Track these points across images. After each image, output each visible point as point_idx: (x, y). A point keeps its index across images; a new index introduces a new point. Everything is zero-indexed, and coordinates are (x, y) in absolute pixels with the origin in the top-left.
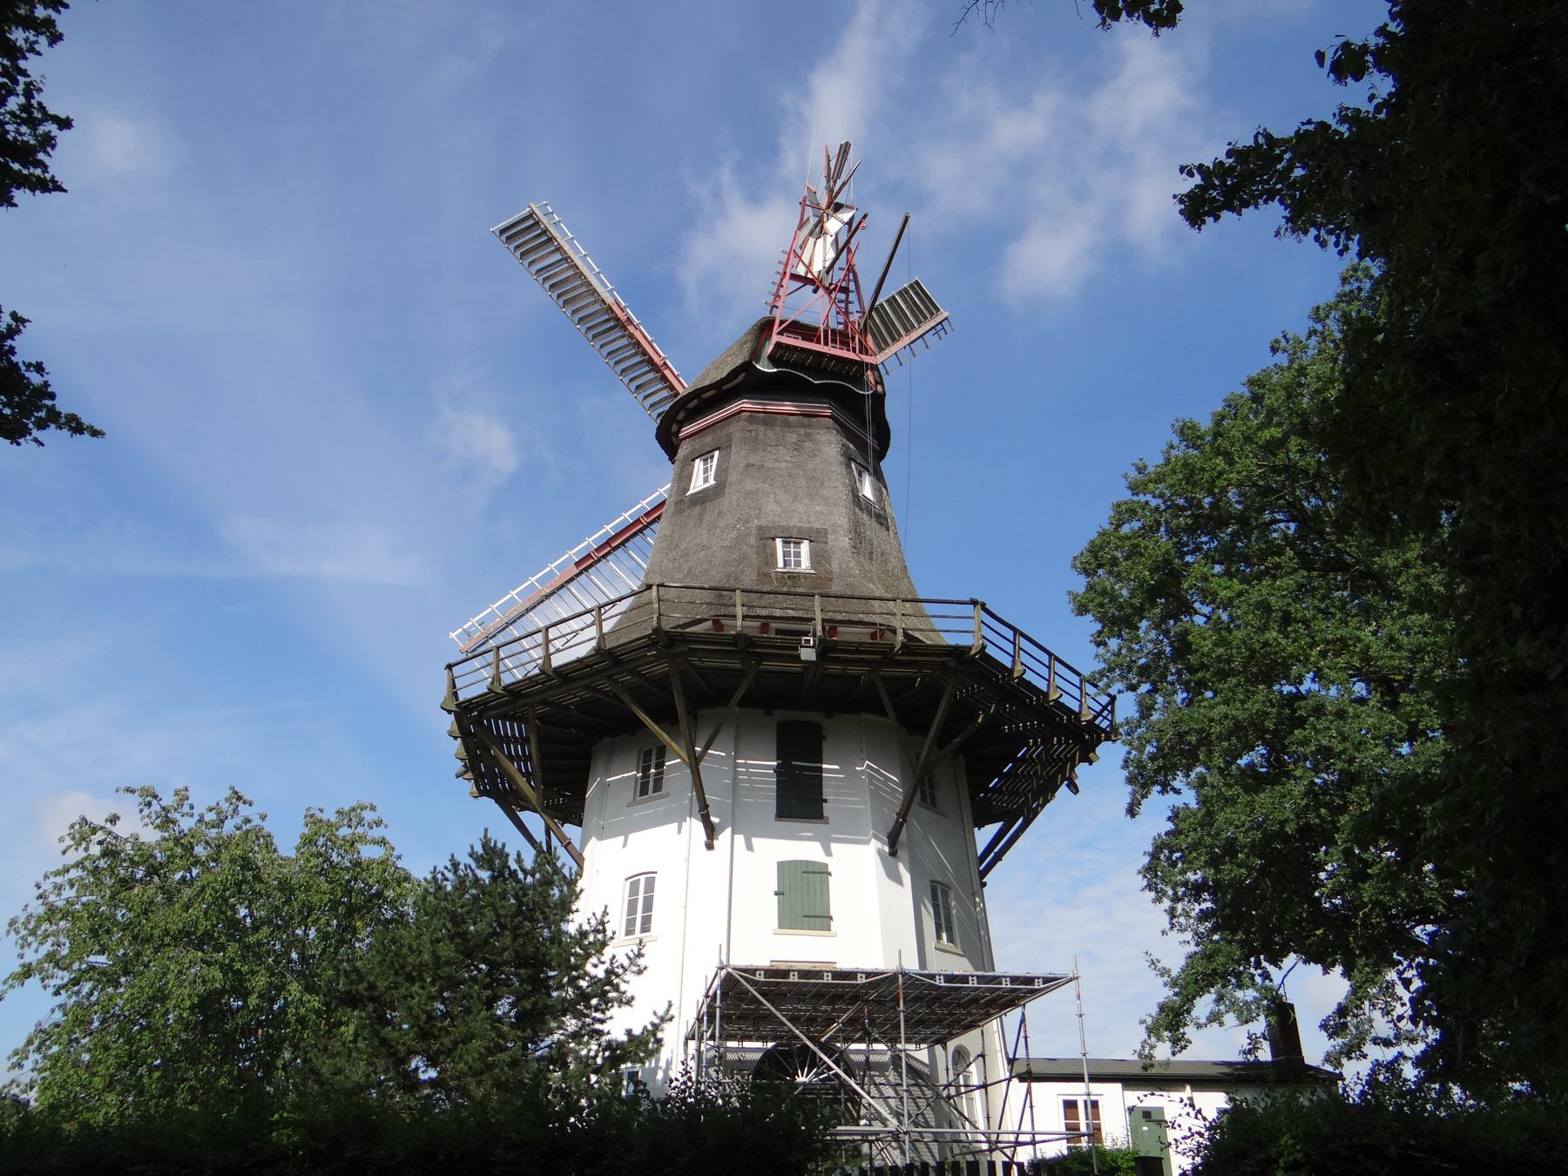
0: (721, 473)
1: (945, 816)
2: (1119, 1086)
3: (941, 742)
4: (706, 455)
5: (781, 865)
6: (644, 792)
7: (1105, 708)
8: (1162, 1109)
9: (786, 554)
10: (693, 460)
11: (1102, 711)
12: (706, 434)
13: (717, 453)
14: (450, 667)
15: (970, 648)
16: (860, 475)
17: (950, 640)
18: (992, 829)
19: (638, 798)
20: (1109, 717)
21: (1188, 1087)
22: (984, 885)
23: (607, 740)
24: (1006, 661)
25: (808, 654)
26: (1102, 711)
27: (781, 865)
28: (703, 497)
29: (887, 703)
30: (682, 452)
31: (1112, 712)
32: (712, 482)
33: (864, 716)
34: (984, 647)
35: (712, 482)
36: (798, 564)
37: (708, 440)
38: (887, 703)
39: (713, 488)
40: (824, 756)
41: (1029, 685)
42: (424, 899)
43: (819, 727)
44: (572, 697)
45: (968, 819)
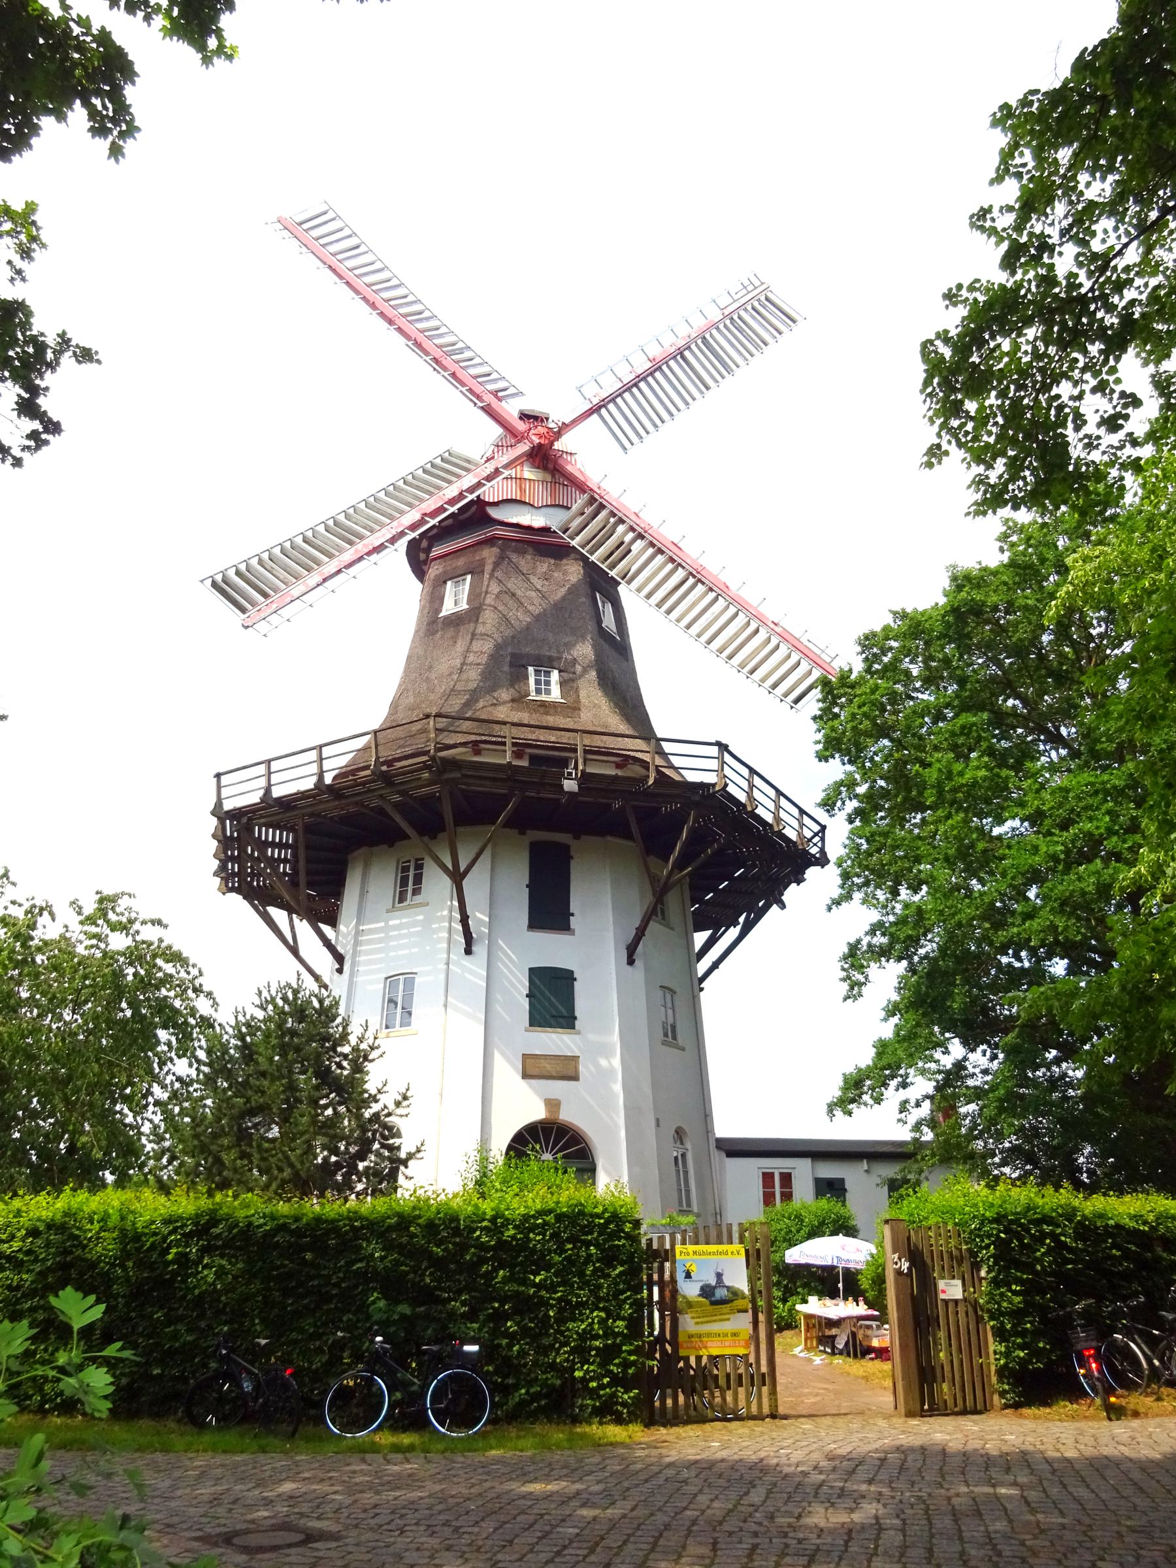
0: (474, 596)
1: (672, 929)
2: (809, 1161)
3: (680, 865)
4: (456, 576)
5: (530, 969)
6: (401, 900)
7: (816, 834)
8: (843, 1180)
9: (538, 682)
10: (445, 582)
11: (813, 837)
12: (458, 557)
13: (469, 577)
14: (218, 776)
15: (714, 785)
16: (603, 603)
17: (692, 777)
18: (707, 934)
19: (397, 905)
20: (819, 844)
21: (865, 1161)
22: (702, 989)
23: (364, 850)
24: (742, 797)
25: (570, 785)
26: (813, 837)
27: (530, 969)
28: (456, 621)
29: (634, 829)
30: (434, 571)
31: (823, 839)
32: (464, 606)
33: (609, 838)
34: (726, 785)
35: (464, 606)
36: (548, 692)
37: (461, 562)
38: (634, 829)
39: (468, 612)
40: (572, 877)
41: (759, 819)
42: (280, 1026)
43: (567, 847)
44: (333, 809)
45: (691, 926)
